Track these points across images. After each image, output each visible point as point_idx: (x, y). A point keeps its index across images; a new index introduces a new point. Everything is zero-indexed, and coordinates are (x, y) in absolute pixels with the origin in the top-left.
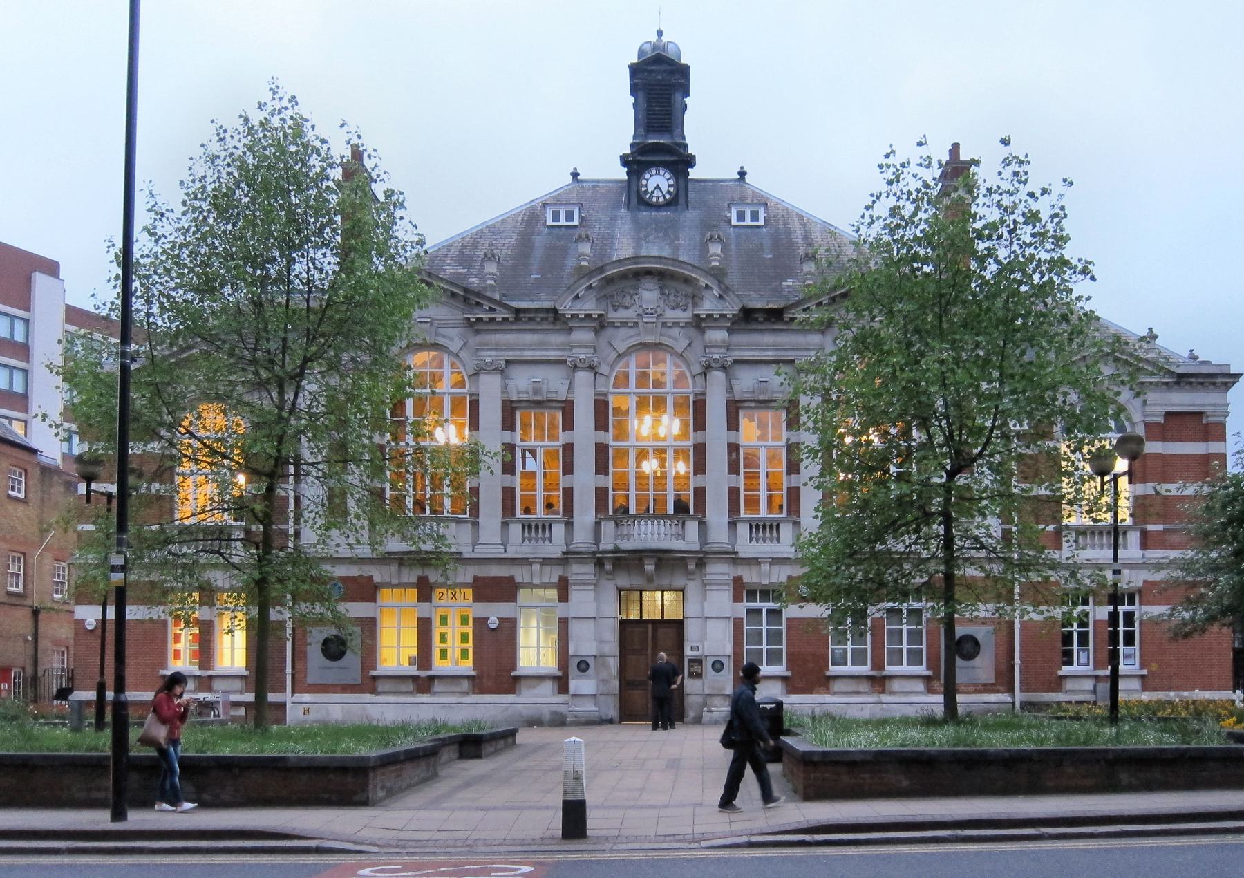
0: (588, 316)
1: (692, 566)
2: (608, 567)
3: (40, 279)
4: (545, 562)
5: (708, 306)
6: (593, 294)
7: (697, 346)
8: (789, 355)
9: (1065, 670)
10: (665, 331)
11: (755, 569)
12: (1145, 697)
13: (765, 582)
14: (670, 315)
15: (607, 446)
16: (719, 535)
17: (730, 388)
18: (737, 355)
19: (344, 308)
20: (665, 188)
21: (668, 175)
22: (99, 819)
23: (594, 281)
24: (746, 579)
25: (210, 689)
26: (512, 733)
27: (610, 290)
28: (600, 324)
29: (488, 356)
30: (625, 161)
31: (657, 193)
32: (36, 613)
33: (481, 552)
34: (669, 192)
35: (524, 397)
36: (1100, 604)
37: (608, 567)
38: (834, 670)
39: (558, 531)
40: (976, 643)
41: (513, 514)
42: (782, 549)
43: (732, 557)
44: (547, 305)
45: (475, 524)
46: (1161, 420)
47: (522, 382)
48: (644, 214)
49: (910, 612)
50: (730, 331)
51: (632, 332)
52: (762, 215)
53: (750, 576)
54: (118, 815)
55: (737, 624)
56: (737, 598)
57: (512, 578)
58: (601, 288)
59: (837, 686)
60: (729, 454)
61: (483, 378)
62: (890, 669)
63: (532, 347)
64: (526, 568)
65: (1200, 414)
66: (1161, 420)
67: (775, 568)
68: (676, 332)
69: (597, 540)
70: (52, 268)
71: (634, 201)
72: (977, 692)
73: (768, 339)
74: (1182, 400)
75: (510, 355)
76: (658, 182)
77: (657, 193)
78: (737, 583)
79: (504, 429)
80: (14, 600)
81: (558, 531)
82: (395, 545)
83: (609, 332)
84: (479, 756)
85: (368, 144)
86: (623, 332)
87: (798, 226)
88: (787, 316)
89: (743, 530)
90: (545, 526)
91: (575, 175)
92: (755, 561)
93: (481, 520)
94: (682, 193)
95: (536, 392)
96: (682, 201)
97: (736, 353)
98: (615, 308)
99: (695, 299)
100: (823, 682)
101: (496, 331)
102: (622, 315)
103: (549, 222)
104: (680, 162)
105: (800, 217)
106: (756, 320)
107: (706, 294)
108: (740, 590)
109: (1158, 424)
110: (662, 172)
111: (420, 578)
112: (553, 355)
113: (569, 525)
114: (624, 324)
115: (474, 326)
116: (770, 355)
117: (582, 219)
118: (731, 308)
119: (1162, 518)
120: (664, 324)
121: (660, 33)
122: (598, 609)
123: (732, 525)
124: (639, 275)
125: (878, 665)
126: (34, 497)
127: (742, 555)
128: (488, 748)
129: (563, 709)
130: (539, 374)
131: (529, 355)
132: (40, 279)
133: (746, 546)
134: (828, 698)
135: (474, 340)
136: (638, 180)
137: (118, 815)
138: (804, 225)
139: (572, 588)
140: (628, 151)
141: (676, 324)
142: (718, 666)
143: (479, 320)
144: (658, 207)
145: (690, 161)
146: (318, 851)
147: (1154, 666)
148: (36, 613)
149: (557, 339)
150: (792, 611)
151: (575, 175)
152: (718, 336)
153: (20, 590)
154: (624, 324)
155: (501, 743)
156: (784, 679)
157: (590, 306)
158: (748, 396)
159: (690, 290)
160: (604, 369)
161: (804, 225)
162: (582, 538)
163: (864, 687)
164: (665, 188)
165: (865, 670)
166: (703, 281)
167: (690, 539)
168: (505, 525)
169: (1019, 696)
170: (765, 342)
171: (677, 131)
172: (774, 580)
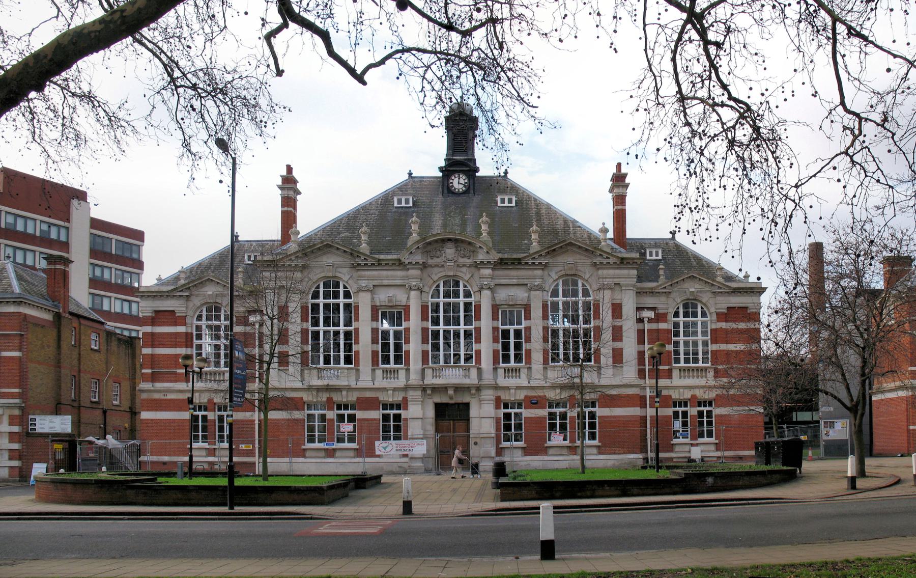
0: (417, 263)
1: (473, 391)
2: (429, 392)
3: (75, 202)
4: (395, 389)
5: (481, 257)
6: (420, 251)
7: (476, 277)
8: (525, 281)
9: (675, 441)
11: (507, 392)
12: (719, 454)
14: (462, 261)
16: (488, 377)
17: (494, 298)
18: (498, 281)
22: (225, 509)
23: (420, 245)
24: (503, 398)
25: (214, 456)
26: (379, 477)
27: (429, 248)
28: (425, 266)
29: (363, 283)
30: (441, 169)
32: (105, 412)
33: (361, 384)
35: (384, 304)
36: (694, 406)
37: (429, 392)
39: (402, 374)
41: (378, 365)
44: (395, 257)
45: (358, 370)
46: (725, 311)
47: (382, 297)
48: (451, 199)
50: (493, 269)
52: (514, 199)
53: (505, 396)
54: (231, 508)
56: (497, 407)
57: (377, 398)
58: (424, 247)
61: (361, 294)
63: (387, 278)
64: (385, 393)
65: (746, 308)
66: (725, 311)
67: (518, 392)
68: (464, 269)
69: (423, 378)
70: (81, 196)
71: (446, 191)
73: (514, 273)
74: (737, 301)
75: (376, 282)
76: (458, 182)
78: (498, 400)
79: (372, 320)
80: (94, 406)
81: (402, 374)
82: (316, 382)
83: (429, 269)
84: (364, 488)
86: (436, 270)
87: (534, 206)
89: (501, 372)
90: (396, 371)
91: (410, 174)
92: (508, 388)
93: (360, 368)
94: (472, 187)
95: (389, 301)
96: (472, 191)
98: (432, 258)
99: (474, 252)
100: (544, 451)
101: (368, 270)
103: (396, 205)
104: (469, 168)
105: (535, 200)
107: (480, 250)
109: (723, 313)
112: (398, 282)
113: (408, 370)
114: (437, 266)
115: (356, 267)
116: (515, 281)
117: (414, 202)
118: (495, 257)
119: (727, 362)
120: (458, 266)
122: (424, 414)
123: (495, 369)
124: (443, 241)
126: (104, 348)
128: (368, 483)
129: (406, 465)
130: (391, 292)
131: (386, 282)
132: (75, 202)
133: (502, 381)
134: (546, 458)
135: (356, 274)
136: (448, 180)
137: (231, 508)
138: (537, 205)
139: (409, 403)
140: (443, 165)
141: (464, 266)
143: (359, 265)
144: (459, 194)
145: (477, 170)
146: (311, 518)
148: (105, 412)
149: (400, 273)
151: (410, 174)
152: (487, 272)
153: (97, 399)
154: (437, 266)
155: (374, 481)
156: (523, 448)
157: (418, 258)
158: (503, 303)
159: (472, 248)
160: (426, 289)
161: (537, 205)
162: (414, 379)
163: (565, 451)
165: (567, 443)
166: (478, 245)
167: (473, 379)
168: (373, 370)
170: (513, 275)
171: (470, 152)
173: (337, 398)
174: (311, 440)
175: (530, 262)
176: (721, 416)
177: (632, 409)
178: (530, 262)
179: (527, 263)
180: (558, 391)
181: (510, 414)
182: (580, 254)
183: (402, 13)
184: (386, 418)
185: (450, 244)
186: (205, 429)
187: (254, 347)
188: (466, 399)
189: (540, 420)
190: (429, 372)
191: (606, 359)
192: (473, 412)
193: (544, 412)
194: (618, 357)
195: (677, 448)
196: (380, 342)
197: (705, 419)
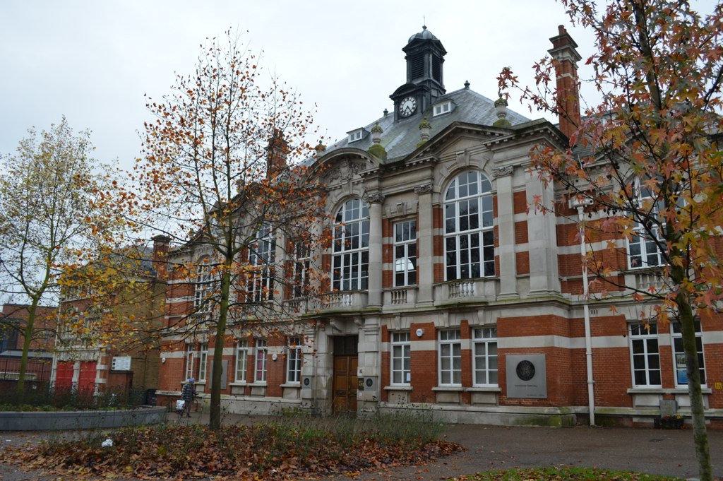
10: (355, 187)
13: (398, 328)
15: (331, 255)
17: (383, 213)
18: (385, 192)
19: (686, 175)
20: (411, 107)
21: (413, 99)
31: (408, 110)
34: (413, 108)
38: (442, 386)
40: (532, 367)
42: (410, 306)
43: (379, 314)
49: (454, 345)
51: (340, 191)
53: (392, 325)
55: (386, 357)
59: (440, 398)
60: (383, 251)
62: (477, 386)
72: (534, 405)
73: (402, 179)
77: (408, 110)
85: (93, 139)
86: (337, 192)
88: (407, 164)
97: (386, 191)
102: (335, 183)
106: (392, 170)
108: (387, 335)
110: (410, 99)
111: (462, 321)
116: (402, 188)
121: (425, 28)
125: (467, 383)
127: (384, 312)
133: (388, 308)
142: (370, 383)
143: (493, 144)
144: (409, 117)
147: (718, 385)
150: (416, 346)
154: (336, 188)
156: (409, 392)
163: (493, 399)
164: (411, 107)
165: (458, 386)
169: (592, 409)
172: (488, 322)
173: (472, 320)
174: (640, 379)
175: (414, 162)
176: (715, 346)
177: (543, 337)
178: (414, 162)
179: (411, 165)
180: (446, 316)
181: (641, 341)
182: (473, 139)
183: (46, 122)
184: (638, 345)
185: (345, 163)
186: (654, 361)
187: (579, 243)
188: (354, 331)
189: (620, 352)
190: (388, 297)
191: (507, 269)
192: (362, 346)
193: (625, 342)
194: (523, 264)
195: (638, 401)
196: (445, 252)
197: (646, 354)
